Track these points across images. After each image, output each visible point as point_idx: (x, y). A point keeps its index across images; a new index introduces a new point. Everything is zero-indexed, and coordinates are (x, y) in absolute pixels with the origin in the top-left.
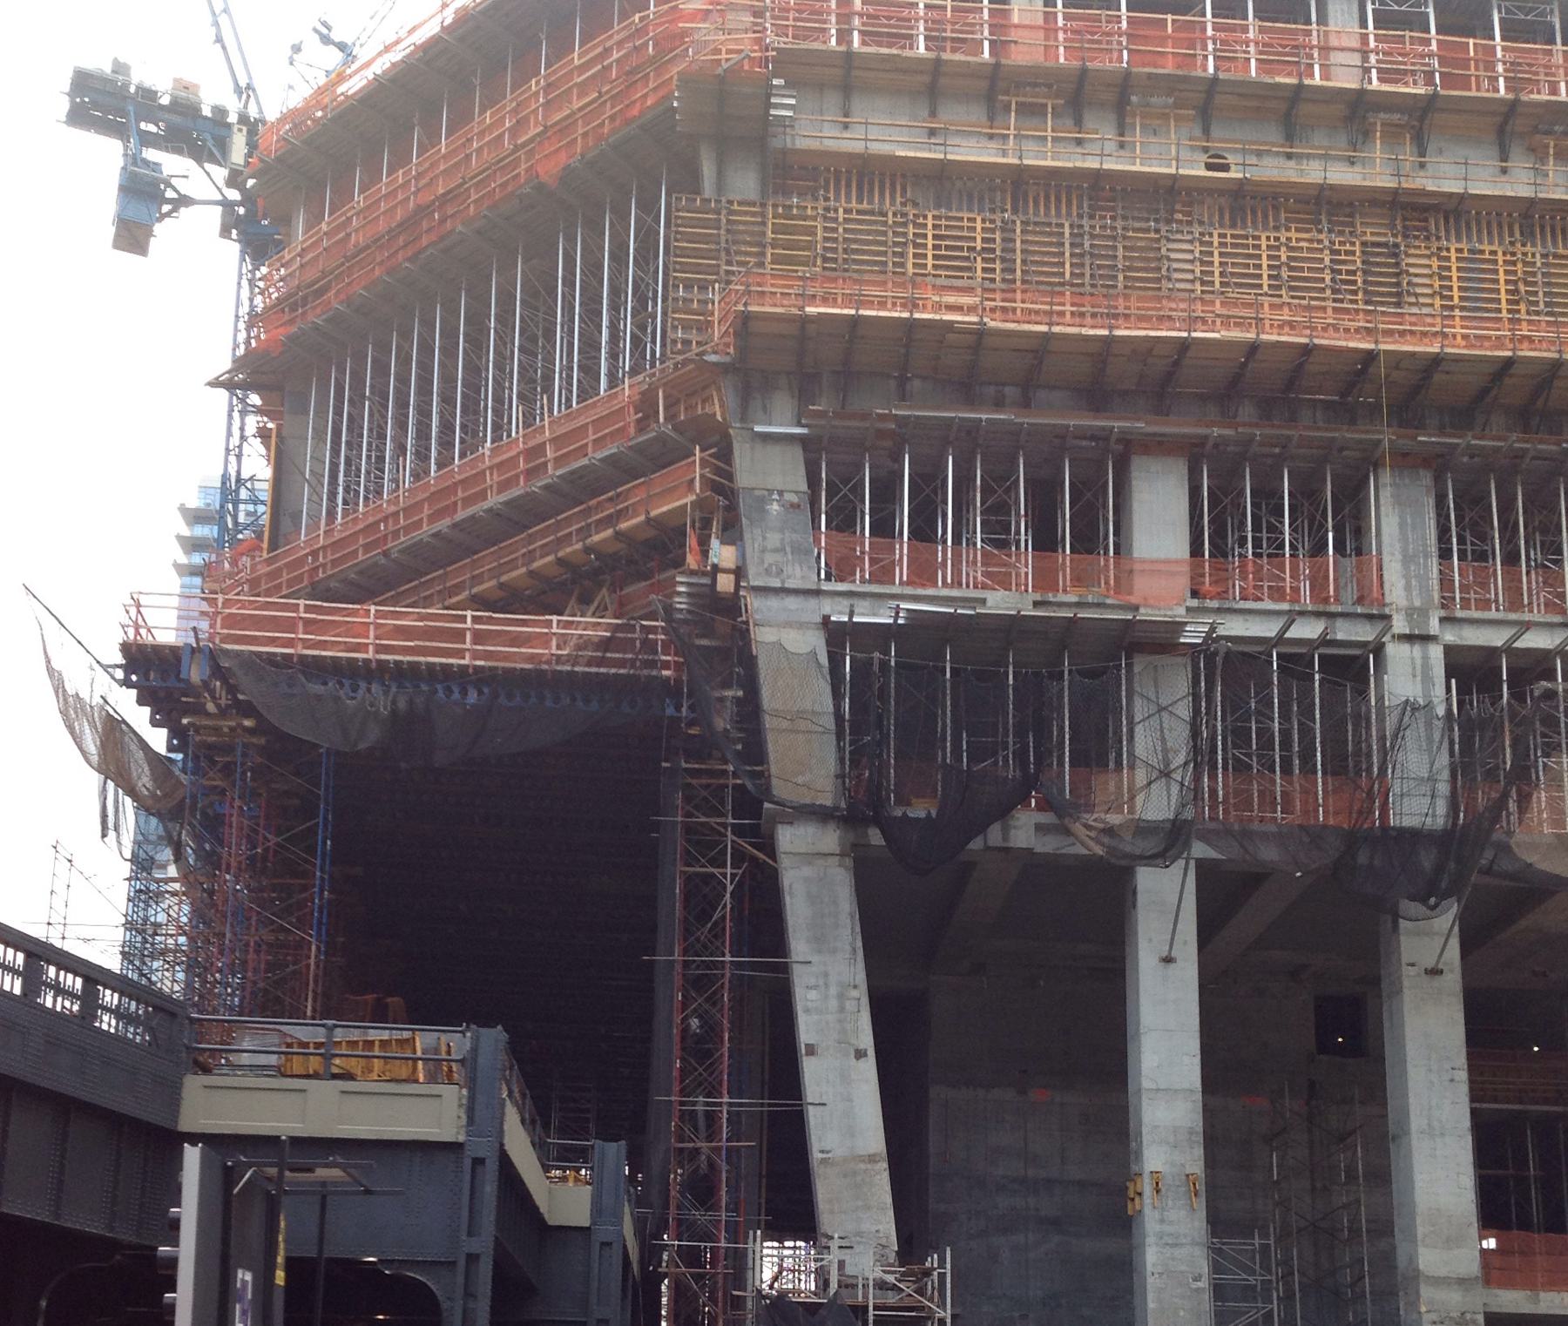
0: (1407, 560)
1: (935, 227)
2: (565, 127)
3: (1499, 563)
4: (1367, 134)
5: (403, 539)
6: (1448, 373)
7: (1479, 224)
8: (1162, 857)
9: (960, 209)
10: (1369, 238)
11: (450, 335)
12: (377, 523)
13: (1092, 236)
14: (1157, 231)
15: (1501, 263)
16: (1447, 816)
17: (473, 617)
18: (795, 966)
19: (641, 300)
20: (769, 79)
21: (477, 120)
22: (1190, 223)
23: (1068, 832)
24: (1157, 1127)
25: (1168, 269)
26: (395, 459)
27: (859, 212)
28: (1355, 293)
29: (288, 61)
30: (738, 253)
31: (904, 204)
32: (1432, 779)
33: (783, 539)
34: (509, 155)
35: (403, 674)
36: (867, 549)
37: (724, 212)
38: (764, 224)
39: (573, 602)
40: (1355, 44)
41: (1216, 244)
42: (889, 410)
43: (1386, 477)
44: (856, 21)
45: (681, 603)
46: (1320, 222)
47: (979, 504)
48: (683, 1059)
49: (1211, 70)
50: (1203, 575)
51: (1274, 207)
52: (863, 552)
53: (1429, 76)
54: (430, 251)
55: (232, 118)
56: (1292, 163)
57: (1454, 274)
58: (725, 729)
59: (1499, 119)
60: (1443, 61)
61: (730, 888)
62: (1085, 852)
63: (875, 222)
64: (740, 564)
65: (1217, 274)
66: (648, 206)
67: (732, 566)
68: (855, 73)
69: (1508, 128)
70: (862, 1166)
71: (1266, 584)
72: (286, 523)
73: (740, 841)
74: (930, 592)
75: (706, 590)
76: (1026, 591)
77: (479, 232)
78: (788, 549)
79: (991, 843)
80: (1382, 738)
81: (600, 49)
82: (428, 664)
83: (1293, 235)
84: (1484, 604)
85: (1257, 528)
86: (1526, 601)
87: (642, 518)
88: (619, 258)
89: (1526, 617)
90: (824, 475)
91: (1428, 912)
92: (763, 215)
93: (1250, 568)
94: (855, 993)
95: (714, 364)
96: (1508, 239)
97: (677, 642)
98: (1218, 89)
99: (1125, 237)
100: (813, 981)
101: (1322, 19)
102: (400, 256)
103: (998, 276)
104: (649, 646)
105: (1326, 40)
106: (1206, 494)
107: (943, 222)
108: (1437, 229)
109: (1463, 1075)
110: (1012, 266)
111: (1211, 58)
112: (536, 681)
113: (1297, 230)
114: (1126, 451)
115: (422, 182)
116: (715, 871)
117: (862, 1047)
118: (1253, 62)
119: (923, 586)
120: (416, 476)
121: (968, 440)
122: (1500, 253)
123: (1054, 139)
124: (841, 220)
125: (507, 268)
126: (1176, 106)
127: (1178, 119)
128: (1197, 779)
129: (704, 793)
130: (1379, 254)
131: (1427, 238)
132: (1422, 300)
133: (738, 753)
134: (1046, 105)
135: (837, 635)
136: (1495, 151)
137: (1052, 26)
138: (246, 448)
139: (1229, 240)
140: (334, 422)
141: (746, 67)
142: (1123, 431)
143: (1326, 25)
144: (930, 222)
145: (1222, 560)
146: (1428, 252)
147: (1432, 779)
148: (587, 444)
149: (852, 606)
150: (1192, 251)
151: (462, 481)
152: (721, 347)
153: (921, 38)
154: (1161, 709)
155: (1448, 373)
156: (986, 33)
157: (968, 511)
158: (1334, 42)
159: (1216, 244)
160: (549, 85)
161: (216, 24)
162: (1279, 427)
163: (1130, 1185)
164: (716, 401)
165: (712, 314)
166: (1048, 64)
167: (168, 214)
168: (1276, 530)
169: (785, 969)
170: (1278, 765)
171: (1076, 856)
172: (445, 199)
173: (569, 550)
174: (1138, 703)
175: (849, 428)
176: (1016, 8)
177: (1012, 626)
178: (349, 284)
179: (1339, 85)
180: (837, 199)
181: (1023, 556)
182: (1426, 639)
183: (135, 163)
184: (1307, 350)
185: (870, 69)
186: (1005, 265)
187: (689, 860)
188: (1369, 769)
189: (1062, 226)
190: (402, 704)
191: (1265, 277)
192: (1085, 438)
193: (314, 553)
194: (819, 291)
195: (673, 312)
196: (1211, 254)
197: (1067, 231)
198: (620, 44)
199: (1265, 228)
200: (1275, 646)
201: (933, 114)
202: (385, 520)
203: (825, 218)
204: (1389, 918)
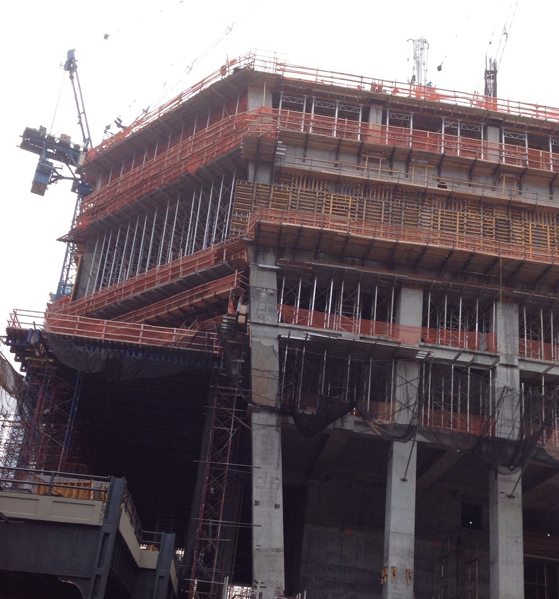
0: (507, 336)
1: (334, 199)
2: (199, 154)
3: (543, 341)
4: (500, 180)
5: (122, 298)
6: (526, 268)
7: (541, 216)
8: (404, 438)
9: (343, 194)
10: (498, 217)
11: (149, 227)
12: (114, 292)
13: (393, 207)
14: (418, 208)
15: (548, 231)
16: (519, 436)
17: (144, 326)
18: (254, 469)
19: (222, 218)
20: (276, 141)
21: (168, 150)
22: (430, 206)
23: (367, 425)
24: (395, 548)
25: (421, 222)
26: (123, 271)
27: (306, 192)
28: (492, 237)
29: (104, 131)
30: (259, 202)
31: (323, 190)
32: (513, 420)
33: (265, 306)
34: (179, 163)
35: (113, 345)
36: (298, 312)
37: (255, 187)
38: (270, 193)
39: (183, 324)
40: (498, 148)
41: (440, 214)
42: (309, 262)
43: (500, 305)
44: (311, 124)
45: (225, 326)
46: (480, 210)
47: (342, 300)
48: (206, 504)
49: (443, 152)
50: (426, 334)
51: (463, 203)
52: (296, 314)
53: (524, 161)
54: (145, 195)
55: (81, 149)
56: (471, 188)
57: (530, 233)
58: (236, 374)
59: (550, 180)
60: (530, 157)
61: (231, 436)
62: (373, 433)
63: (312, 196)
64: (248, 312)
65: (439, 225)
66: (228, 184)
67: (245, 313)
68: (309, 142)
69: (554, 183)
70: (273, 553)
71: (451, 340)
72: (80, 291)
73: (237, 418)
74: (320, 330)
75: (234, 322)
76: (358, 333)
77: (164, 190)
78: (267, 310)
79: (336, 427)
80: (494, 402)
81: (216, 127)
82: (124, 342)
83: (469, 213)
84: (537, 357)
85: (448, 319)
86: (553, 356)
87: (213, 295)
88: (215, 203)
89: (552, 362)
90: (284, 284)
91: (509, 471)
92: (270, 190)
93: (445, 333)
94: (277, 482)
95: (246, 241)
96: (551, 223)
97: (222, 341)
98: (445, 159)
99: (405, 209)
100: (261, 475)
101: (485, 138)
102: (134, 197)
103: (356, 218)
104: (211, 342)
105: (487, 146)
106: (429, 304)
107: (337, 198)
108: (525, 217)
109: (521, 540)
110: (362, 216)
111: (443, 148)
112: (164, 351)
113: (471, 212)
114: (400, 285)
115: (145, 171)
116: (227, 429)
117: (278, 503)
118: (459, 150)
119: (318, 327)
120: (131, 276)
121: (340, 276)
122: (548, 228)
123: (382, 172)
124: (299, 194)
125: (173, 204)
126: (428, 164)
127: (429, 168)
128: (420, 408)
129: (226, 399)
130: (502, 224)
131: (521, 220)
132: (517, 242)
133: (239, 383)
134: (379, 160)
135: (283, 342)
136: (548, 191)
137: (384, 131)
138: (71, 266)
139: (445, 213)
140: (103, 256)
141: (269, 136)
142: (399, 278)
143: (487, 140)
144: (332, 197)
145: (434, 329)
146: (521, 225)
147: (513, 420)
148: (195, 267)
149: (290, 332)
150: (431, 216)
151: (147, 278)
152: (249, 235)
153: (335, 132)
154: (407, 382)
155: (526, 268)
156: (359, 132)
157: (338, 303)
158: (489, 146)
159: (440, 214)
160: (195, 139)
161: (80, 117)
162: (460, 282)
163: (383, 572)
164: (245, 254)
165: (247, 223)
166: (383, 144)
167: (53, 182)
168: (456, 321)
169: (250, 470)
170: (452, 409)
171: (370, 435)
172: (154, 177)
173: (184, 305)
174: (398, 379)
175: (294, 268)
176: (371, 124)
177: (351, 345)
178: (114, 206)
179: (490, 162)
180: (298, 186)
181: (357, 320)
182: (513, 366)
183: (43, 162)
184: (472, 255)
185: (316, 141)
186: (359, 215)
187: (217, 424)
188: (488, 414)
189: (382, 203)
190: (111, 356)
191: (458, 228)
192: (384, 279)
193: (89, 302)
194: (288, 217)
195: (233, 222)
196: (438, 218)
197: (383, 205)
198: (223, 125)
199: (459, 210)
200: (453, 363)
201: (337, 159)
202: (117, 291)
203: (293, 193)
204: (494, 472)
